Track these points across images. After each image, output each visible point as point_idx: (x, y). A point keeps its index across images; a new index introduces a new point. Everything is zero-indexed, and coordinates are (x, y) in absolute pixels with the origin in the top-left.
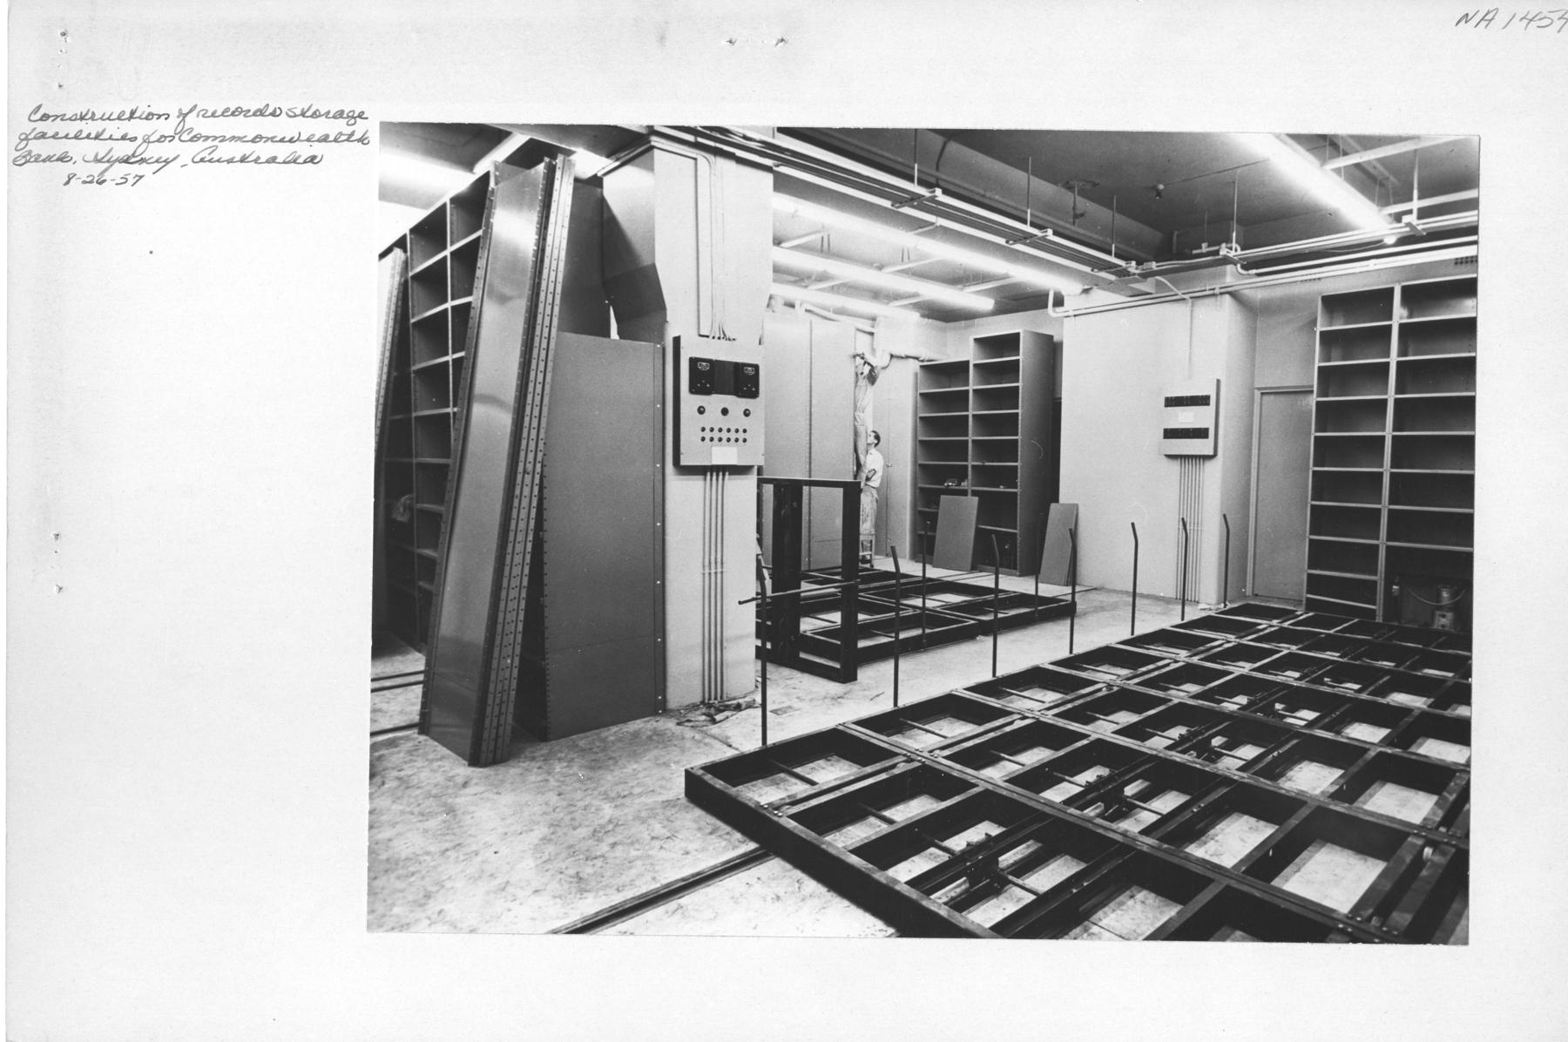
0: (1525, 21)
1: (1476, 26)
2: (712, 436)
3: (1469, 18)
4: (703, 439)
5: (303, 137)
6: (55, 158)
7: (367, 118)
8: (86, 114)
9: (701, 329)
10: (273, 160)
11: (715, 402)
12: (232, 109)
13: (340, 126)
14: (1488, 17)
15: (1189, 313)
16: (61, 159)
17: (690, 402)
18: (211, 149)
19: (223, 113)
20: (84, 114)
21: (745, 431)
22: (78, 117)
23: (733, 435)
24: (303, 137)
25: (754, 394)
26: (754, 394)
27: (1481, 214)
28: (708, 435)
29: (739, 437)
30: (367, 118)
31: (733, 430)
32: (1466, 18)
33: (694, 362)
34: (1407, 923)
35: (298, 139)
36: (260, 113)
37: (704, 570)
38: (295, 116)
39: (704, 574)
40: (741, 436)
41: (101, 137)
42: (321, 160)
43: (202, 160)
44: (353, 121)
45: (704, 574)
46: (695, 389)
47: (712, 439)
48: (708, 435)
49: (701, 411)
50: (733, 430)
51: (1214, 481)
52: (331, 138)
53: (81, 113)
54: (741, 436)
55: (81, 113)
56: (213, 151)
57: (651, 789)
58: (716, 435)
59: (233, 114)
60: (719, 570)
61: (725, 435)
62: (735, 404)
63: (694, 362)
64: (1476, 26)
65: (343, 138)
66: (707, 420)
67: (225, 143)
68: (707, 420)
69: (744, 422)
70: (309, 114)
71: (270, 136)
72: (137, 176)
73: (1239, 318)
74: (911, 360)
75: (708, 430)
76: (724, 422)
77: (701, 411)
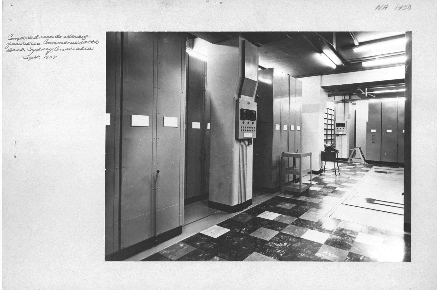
2: (339, 131)
3: (380, 7)
5: (79, 42)
6: (19, 50)
8: (71, 49)
10: (78, 49)
11: (339, 128)
14: (386, 7)
15: (320, 79)
16: (21, 50)
17: (336, 128)
18: (11, 35)
20: (70, 49)
22: (68, 49)
24: (79, 42)
29: (343, 131)
34: (404, 122)
35: (78, 43)
37: (239, 169)
39: (239, 171)
40: (343, 131)
42: (93, 49)
45: (239, 171)
46: (337, 126)
49: (243, 123)
51: (157, 188)
53: (69, 48)
54: (343, 131)
55: (69, 48)
56: (12, 36)
58: (339, 131)
60: (246, 169)
61: (341, 131)
62: (342, 128)
63: (337, 123)
65: (90, 42)
67: (56, 44)
69: (343, 129)
72: (55, 56)
73: (335, 78)
74: (25, 58)
76: (341, 129)
77: (243, 123)
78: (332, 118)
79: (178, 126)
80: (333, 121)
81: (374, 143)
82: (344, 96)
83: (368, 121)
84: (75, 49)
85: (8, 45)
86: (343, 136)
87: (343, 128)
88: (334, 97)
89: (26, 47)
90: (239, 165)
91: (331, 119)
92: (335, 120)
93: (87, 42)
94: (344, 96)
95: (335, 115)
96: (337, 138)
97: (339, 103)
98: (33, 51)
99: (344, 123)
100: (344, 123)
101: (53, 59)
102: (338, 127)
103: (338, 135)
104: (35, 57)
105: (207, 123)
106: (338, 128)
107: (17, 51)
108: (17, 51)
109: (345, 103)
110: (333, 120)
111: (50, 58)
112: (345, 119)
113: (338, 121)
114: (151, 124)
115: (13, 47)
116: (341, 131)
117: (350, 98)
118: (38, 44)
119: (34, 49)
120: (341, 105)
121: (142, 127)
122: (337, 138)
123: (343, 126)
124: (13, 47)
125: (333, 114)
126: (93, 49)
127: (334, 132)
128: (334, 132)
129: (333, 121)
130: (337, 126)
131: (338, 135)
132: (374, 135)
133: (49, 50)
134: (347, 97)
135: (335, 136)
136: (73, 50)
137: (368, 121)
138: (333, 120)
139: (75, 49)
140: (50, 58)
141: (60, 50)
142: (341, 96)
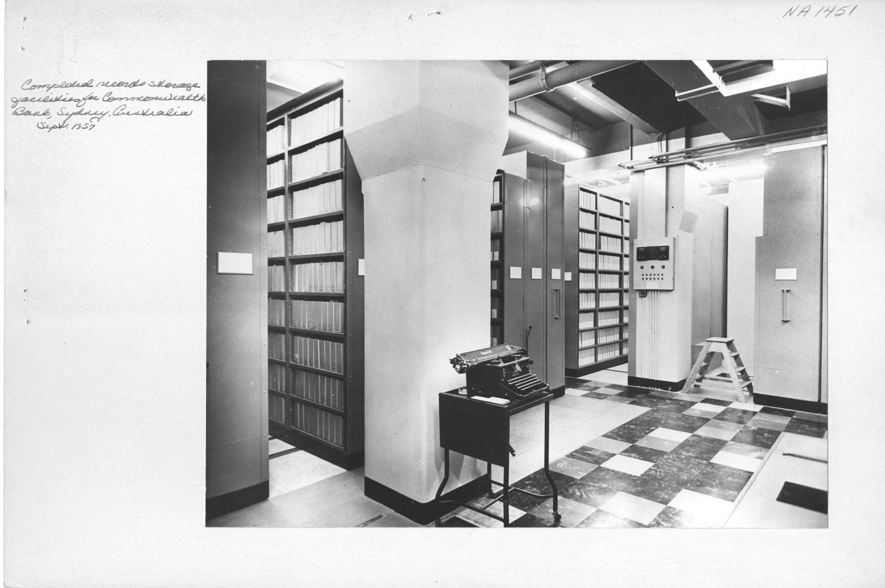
0: (828, 12)
1: (815, 16)
2: (645, 277)
3: (788, 14)
4: (643, 279)
7: (199, 87)
9: (620, 224)
12: (118, 83)
13: (183, 92)
17: (637, 264)
18: (29, 81)
19: (32, 99)
20: (144, 112)
21: (662, 275)
23: (656, 277)
25: (667, 258)
26: (667, 258)
27: (828, 136)
28: (645, 277)
30: (199, 87)
31: (653, 274)
32: (791, 12)
33: (638, 249)
36: (134, 84)
38: (155, 86)
40: (660, 277)
41: (190, 99)
42: (190, 114)
43: (117, 115)
44: (189, 89)
46: (639, 259)
47: (647, 279)
48: (645, 277)
50: (653, 274)
52: (185, 98)
54: (660, 277)
57: (528, 328)
58: (649, 277)
59: (118, 85)
61: (653, 277)
62: (657, 263)
64: (815, 16)
66: (644, 271)
68: (644, 271)
70: (164, 84)
71: (158, 100)
75: (656, 279)
78: (622, 233)
79: (253, 271)
80: (627, 226)
81: (787, 324)
82: (664, 142)
83: (761, 234)
84: (155, 113)
85: (15, 102)
86: (663, 296)
87: (663, 267)
88: (627, 371)
89: (54, 107)
90: (557, 303)
91: (619, 234)
92: (631, 239)
93: (185, 98)
94: (664, 142)
95: (633, 222)
96: (642, 306)
97: (646, 171)
98: (68, 116)
99: (667, 248)
100: (667, 248)
101: (90, 130)
102: (644, 263)
103: (644, 293)
104: (58, 126)
105: (358, 261)
106: (642, 268)
107: (34, 115)
108: (34, 115)
109: (668, 167)
110: (627, 239)
111: (83, 128)
112: (670, 232)
113: (643, 241)
114: (548, 270)
115: (29, 106)
116: (653, 277)
117: (688, 144)
118: (33, 88)
119: (70, 113)
120: (656, 177)
121: (237, 275)
122: (642, 306)
123: (660, 259)
124: (29, 106)
125: (628, 218)
126: (190, 114)
127: (631, 282)
128: (631, 282)
129: (627, 225)
130: (639, 259)
131: (644, 293)
132: (788, 291)
133: (101, 114)
134: (678, 144)
135: (633, 296)
136: (149, 115)
137: (761, 234)
138: (627, 239)
139: (155, 113)
140: (83, 128)
141: (128, 114)
142: (656, 143)
